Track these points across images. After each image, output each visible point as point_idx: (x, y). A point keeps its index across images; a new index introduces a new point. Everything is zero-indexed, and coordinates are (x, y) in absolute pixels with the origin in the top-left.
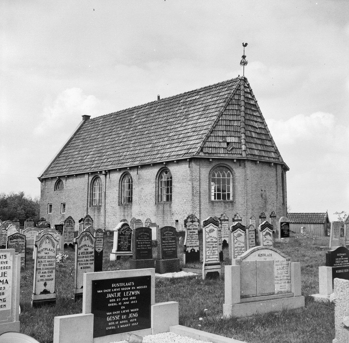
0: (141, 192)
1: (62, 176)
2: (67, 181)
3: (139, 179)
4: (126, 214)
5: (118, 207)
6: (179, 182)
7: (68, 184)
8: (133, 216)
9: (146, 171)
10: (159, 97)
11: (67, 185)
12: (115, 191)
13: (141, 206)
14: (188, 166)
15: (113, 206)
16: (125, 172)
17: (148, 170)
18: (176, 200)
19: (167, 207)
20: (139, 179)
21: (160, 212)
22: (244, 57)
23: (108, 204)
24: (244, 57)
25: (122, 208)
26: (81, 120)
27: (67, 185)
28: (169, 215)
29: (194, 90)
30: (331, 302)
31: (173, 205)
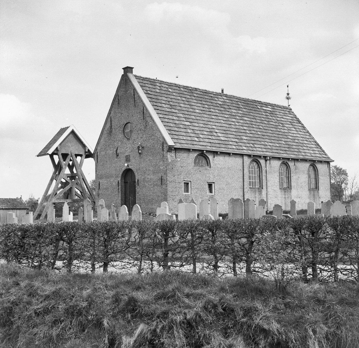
0: (298, 179)
1: (179, 148)
2: (216, 158)
3: (296, 169)
4: (287, 196)
5: (279, 190)
6: (322, 176)
7: (217, 161)
8: (292, 199)
9: (301, 164)
10: (222, 90)
11: (216, 162)
12: (276, 176)
13: (299, 191)
14: (327, 166)
15: (275, 189)
16: (285, 162)
17: (302, 164)
18: (322, 188)
19: (316, 192)
20: (296, 169)
21: (312, 196)
22: (288, 94)
23: (270, 187)
24: (288, 94)
25: (283, 193)
26: (123, 70)
27: (216, 162)
28: (318, 198)
29: (270, 103)
30: (236, 264)
31: (320, 191)
